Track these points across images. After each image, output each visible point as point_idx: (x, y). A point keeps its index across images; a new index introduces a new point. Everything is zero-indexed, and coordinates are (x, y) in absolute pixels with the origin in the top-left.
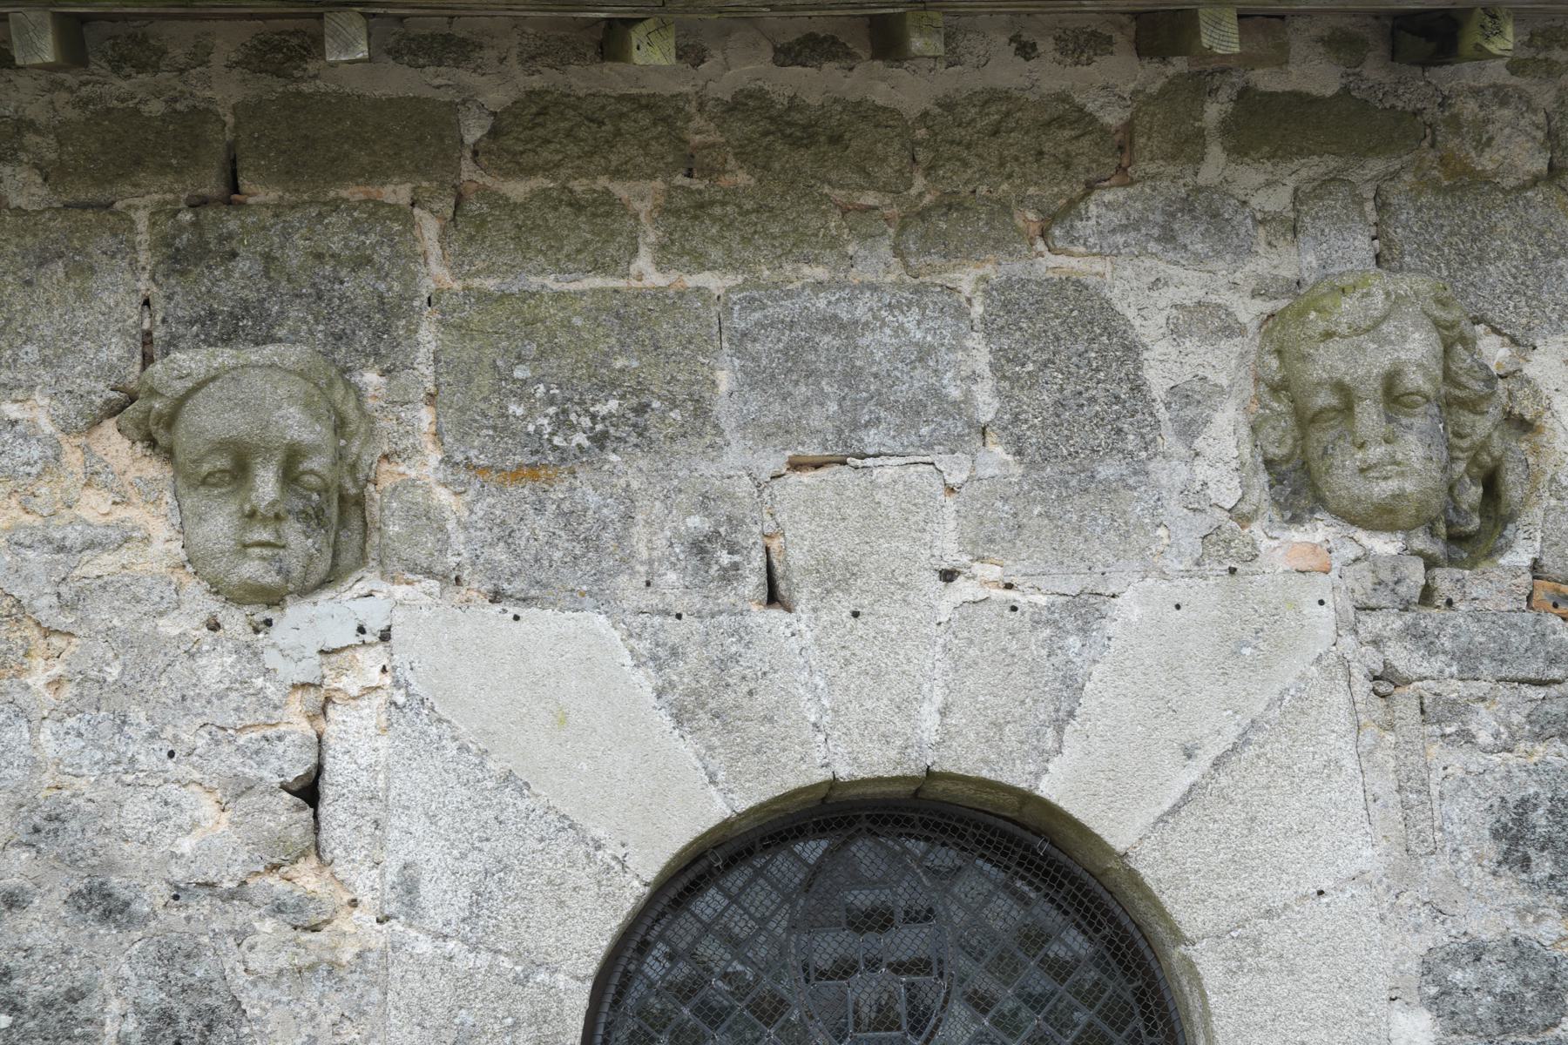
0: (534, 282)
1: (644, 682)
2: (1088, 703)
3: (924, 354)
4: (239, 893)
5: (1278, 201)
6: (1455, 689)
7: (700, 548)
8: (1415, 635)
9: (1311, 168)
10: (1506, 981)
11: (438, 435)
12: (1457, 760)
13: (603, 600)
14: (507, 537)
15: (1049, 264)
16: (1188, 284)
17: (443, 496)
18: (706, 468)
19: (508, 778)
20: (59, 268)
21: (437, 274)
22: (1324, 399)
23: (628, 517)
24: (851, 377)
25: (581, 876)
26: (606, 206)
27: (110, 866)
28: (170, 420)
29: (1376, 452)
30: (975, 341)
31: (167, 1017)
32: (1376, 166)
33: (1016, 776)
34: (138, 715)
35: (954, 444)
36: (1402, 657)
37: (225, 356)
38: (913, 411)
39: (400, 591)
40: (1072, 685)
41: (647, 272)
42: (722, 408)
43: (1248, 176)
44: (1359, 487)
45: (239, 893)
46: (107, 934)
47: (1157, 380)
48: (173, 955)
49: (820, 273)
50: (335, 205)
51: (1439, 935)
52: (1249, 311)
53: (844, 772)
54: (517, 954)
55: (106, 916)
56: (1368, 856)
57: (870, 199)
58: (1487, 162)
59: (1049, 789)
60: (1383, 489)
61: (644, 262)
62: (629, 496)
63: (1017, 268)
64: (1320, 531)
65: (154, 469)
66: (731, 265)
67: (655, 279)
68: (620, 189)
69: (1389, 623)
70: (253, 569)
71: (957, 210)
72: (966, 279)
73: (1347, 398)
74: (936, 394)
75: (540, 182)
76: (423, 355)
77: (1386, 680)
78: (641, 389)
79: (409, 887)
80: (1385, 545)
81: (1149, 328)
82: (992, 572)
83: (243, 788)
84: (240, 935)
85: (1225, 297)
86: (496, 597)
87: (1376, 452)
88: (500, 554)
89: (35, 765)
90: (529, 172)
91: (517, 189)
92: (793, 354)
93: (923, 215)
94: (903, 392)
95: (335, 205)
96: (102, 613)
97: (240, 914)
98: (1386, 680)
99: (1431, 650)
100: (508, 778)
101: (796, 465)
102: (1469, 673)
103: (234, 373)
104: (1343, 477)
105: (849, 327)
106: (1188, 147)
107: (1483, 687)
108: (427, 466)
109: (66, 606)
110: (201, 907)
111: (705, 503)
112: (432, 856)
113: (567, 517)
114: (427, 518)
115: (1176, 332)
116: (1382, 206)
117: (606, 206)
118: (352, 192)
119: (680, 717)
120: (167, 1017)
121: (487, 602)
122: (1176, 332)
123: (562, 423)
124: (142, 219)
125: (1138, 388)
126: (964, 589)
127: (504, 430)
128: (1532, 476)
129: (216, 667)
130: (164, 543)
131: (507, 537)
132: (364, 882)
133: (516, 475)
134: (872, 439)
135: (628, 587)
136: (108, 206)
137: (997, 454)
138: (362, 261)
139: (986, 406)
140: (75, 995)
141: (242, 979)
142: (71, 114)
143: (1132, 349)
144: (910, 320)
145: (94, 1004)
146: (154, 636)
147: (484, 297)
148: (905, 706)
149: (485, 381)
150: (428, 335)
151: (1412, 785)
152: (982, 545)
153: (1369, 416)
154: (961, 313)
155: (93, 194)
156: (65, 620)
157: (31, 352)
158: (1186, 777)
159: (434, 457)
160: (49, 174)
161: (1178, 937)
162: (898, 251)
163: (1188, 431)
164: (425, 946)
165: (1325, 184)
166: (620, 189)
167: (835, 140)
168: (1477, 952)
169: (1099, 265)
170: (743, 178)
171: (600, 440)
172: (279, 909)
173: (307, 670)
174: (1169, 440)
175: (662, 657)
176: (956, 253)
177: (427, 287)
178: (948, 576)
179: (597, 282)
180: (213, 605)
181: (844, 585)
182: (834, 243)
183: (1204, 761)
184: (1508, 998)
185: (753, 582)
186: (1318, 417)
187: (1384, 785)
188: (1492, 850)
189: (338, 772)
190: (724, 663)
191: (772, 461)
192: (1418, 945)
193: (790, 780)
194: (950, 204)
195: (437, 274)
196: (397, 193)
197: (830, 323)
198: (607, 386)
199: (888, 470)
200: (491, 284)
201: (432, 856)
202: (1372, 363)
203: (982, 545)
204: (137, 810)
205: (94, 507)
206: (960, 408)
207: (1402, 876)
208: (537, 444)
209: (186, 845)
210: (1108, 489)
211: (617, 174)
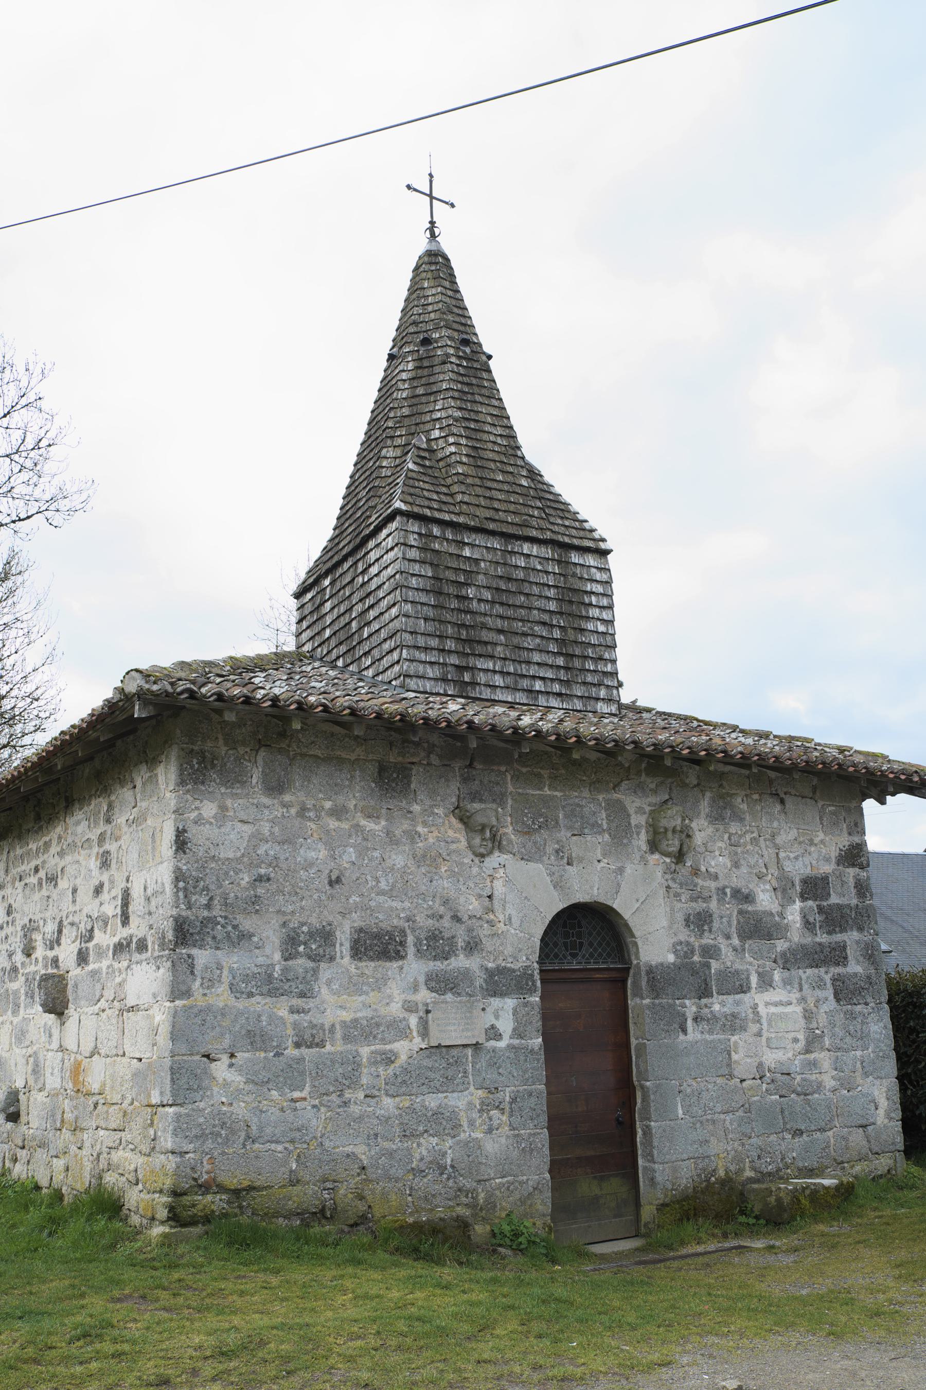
0: (528, 791)
1: (548, 879)
2: (621, 889)
3: (595, 813)
4: (480, 918)
5: (653, 786)
6: (679, 890)
7: (557, 851)
8: (673, 879)
9: (659, 779)
10: (685, 949)
11: (512, 823)
12: (679, 905)
13: (542, 862)
14: (524, 847)
15: (616, 796)
16: (638, 803)
17: (513, 836)
18: (558, 835)
19: (526, 898)
20: (443, 780)
21: (510, 788)
22: (662, 830)
23: (545, 844)
24: (582, 817)
25: (538, 918)
26: (539, 776)
27: (458, 911)
28: (469, 817)
29: (670, 842)
30: (603, 811)
31: (469, 943)
32: (670, 780)
33: (609, 903)
34: (461, 879)
35: (600, 833)
36: (671, 883)
37: (483, 806)
38: (593, 826)
39: (505, 856)
40: (619, 885)
41: (548, 792)
42: (561, 822)
43: (649, 780)
44: (666, 848)
45: (480, 918)
46: (458, 925)
47: (633, 822)
48: (470, 930)
49: (576, 794)
50: (493, 770)
51: (675, 940)
52: (648, 809)
53: (582, 900)
54: (528, 934)
55: (457, 921)
56: (665, 923)
57: (584, 778)
58: (687, 781)
59: (615, 906)
60: (671, 849)
61: (546, 789)
62: (545, 840)
63: (609, 796)
64: (656, 856)
65: (460, 826)
66: (561, 791)
67: (548, 792)
68: (542, 772)
69: (668, 876)
70: (482, 850)
71: (363, 1245)
72: (601, 797)
73: (666, 830)
74: (596, 822)
75: (529, 769)
76: (509, 806)
77: (668, 887)
78: (546, 817)
79: (510, 919)
80: (668, 860)
81: (632, 811)
82: (606, 861)
83: (480, 896)
84: (481, 927)
85: (644, 806)
86: (522, 859)
87: (670, 842)
88: (523, 850)
89: (444, 889)
90: (527, 766)
91: (524, 770)
92: (573, 811)
93: (594, 783)
94: (591, 821)
95: (493, 770)
96: (454, 857)
97: (481, 922)
98: (668, 887)
99: (676, 883)
100: (526, 898)
101: (574, 835)
102: (681, 888)
103: (484, 810)
104: (663, 846)
105: (581, 806)
106: (639, 773)
107: (683, 890)
108: (509, 830)
109: (448, 855)
110: (474, 921)
111: (558, 842)
112: (514, 913)
113: (535, 843)
114: (510, 842)
115: (636, 813)
116: (670, 789)
117: (539, 776)
118: (495, 768)
119: (555, 887)
120: (469, 943)
121: (153, 991)
122: (636, 813)
123: (533, 823)
124: (457, 769)
125: (630, 824)
126: (602, 864)
127: (523, 823)
128: (689, 847)
129: (475, 870)
130: (464, 843)
131: (524, 847)
132: (501, 917)
133: (526, 833)
134: (586, 831)
135: (545, 858)
136: (449, 765)
137: (607, 836)
138: (498, 784)
139: (605, 826)
140: (453, 937)
141: (482, 936)
142: (443, 743)
143: (629, 815)
144: (592, 806)
145: (456, 939)
146: (463, 863)
147: (519, 794)
148: (592, 888)
149: (520, 812)
150: (510, 802)
151: (672, 909)
152: (604, 855)
153: (670, 834)
154: (601, 805)
155: (448, 763)
156: (448, 858)
157: (439, 798)
158: (637, 905)
159: (511, 828)
160: (440, 757)
161: (633, 936)
162: (590, 791)
163: (638, 834)
164: (513, 931)
165: (662, 783)
166: (542, 772)
167: (580, 765)
168: (681, 943)
169: (624, 797)
170: (563, 772)
171: (540, 827)
172: (488, 922)
173: (489, 873)
174: (635, 836)
175: (551, 874)
176: (599, 792)
177: (509, 790)
178: (599, 861)
179: (538, 792)
180: (472, 857)
181: (581, 862)
182: (579, 788)
183: (640, 901)
184: (686, 952)
185: (565, 860)
186: (660, 833)
187: (668, 909)
188: (684, 923)
189: (496, 893)
190: (562, 876)
191: (569, 835)
192: (672, 941)
193: (573, 902)
194: (599, 781)
195: (510, 788)
196: (503, 769)
197: (578, 805)
198: (541, 815)
199: (589, 838)
200: (520, 791)
201: (514, 913)
202: (672, 824)
203: (604, 855)
204: (462, 900)
205: (450, 833)
206: (600, 826)
207: (670, 928)
208: (529, 827)
209: (471, 907)
210: (625, 845)
211: (541, 768)
